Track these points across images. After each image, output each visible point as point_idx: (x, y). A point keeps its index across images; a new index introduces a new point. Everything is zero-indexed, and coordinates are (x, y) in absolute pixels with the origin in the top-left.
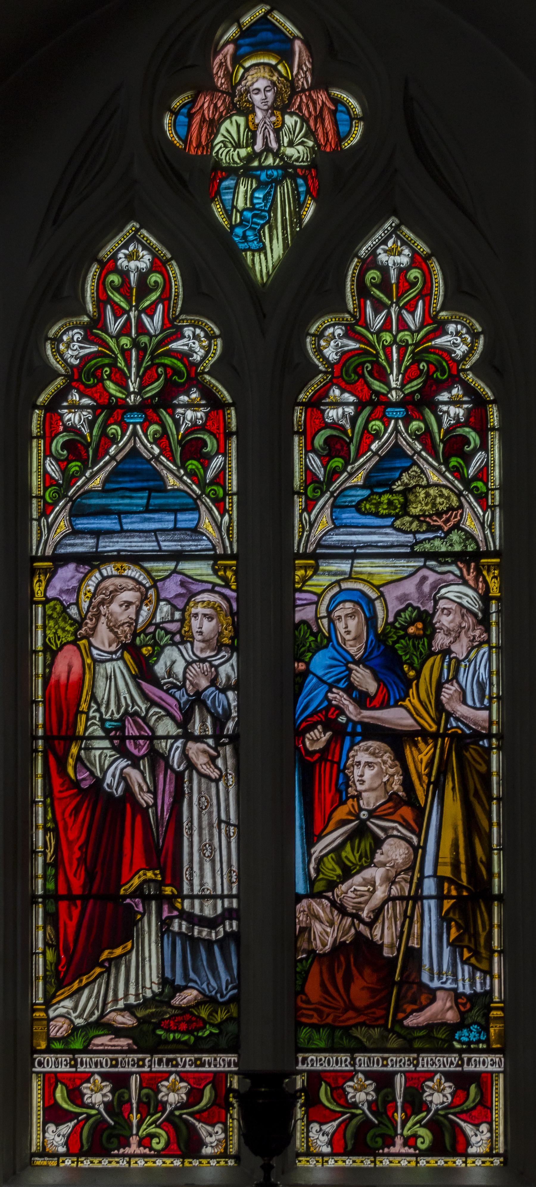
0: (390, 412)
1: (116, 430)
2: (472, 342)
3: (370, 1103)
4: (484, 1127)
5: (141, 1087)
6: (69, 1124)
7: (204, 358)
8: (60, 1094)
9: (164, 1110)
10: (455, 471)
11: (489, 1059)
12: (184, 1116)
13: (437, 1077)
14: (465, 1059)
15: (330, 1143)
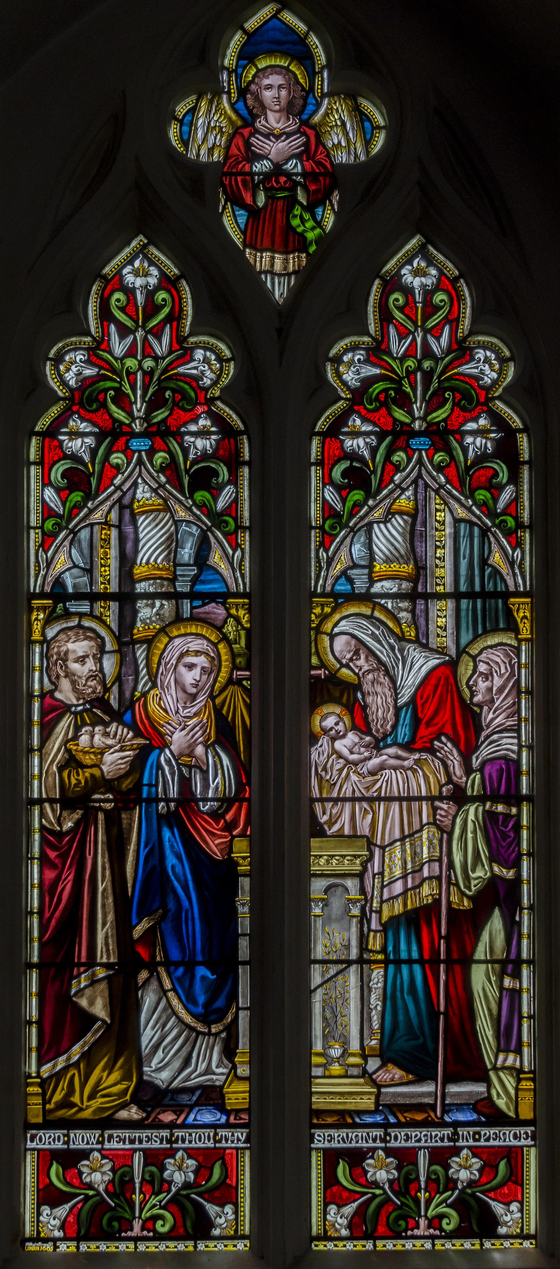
0: (414, 443)
1: (160, 457)
2: (501, 369)
3: (391, 1182)
4: (514, 1207)
5: (145, 1165)
6: (352, 1204)
7: (215, 383)
8: (342, 1171)
9: (169, 1191)
10: (482, 506)
11: (403, 1134)
12: (193, 1196)
13: (465, 1151)
14: (106, 1136)
15: (350, 1226)
